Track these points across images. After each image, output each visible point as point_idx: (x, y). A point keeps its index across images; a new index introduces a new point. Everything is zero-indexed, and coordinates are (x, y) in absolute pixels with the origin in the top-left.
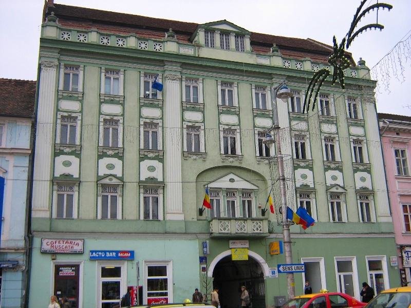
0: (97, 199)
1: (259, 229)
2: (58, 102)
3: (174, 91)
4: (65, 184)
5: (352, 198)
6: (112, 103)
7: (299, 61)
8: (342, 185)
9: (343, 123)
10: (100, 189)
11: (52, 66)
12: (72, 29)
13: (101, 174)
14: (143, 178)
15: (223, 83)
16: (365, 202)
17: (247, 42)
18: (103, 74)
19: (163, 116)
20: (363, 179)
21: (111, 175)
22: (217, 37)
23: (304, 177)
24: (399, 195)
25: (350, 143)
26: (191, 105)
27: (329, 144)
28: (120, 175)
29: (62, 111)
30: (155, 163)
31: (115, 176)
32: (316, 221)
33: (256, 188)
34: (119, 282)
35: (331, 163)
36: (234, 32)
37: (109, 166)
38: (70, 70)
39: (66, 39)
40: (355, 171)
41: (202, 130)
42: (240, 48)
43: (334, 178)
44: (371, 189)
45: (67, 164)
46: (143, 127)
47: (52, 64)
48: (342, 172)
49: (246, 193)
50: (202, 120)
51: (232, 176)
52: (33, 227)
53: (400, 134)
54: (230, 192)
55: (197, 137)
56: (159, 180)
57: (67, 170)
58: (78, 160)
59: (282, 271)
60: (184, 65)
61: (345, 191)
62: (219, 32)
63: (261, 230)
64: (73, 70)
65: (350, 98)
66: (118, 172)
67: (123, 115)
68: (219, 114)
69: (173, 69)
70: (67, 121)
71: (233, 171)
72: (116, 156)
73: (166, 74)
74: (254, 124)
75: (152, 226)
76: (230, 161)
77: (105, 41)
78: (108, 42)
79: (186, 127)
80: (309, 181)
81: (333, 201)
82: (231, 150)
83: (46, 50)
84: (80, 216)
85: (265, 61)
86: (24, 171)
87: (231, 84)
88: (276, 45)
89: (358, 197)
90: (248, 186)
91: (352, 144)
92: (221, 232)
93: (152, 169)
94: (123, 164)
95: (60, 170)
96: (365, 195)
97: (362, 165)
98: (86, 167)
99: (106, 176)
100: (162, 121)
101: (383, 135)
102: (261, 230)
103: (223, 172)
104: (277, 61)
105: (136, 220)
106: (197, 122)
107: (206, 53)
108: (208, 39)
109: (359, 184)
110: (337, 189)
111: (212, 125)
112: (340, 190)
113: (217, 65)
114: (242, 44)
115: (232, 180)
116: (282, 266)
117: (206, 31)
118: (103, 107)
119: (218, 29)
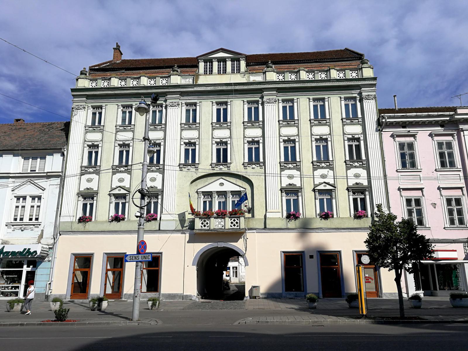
1: (207, 226)
2: (85, 134)
3: (272, 112)
4: (88, 196)
6: (95, 132)
10: (317, 193)
11: (175, 105)
12: (98, 78)
13: (317, 182)
17: (243, 63)
18: (120, 110)
19: (103, 138)
20: (290, 177)
27: (289, 146)
28: (332, 182)
30: (325, 171)
31: (328, 184)
33: (127, 192)
36: (228, 58)
38: (317, 102)
39: (135, 85)
41: (329, 141)
42: (236, 70)
44: (300, 186)
45: (89, 181)
46: (347, 141)
48: (131, 175)
50: (329, 133)
54: (221, 194)
57: (89, 185)
58: (129, 176)
59: (129, 260)
60: (88, 97)
68: (213, 129)
70: (288, 143)
71: (224, 177)
72: (158, 171)
73: (169, 101)
74: (181, 137)
75: (115, 226)
77: (123, 83)
78: (290, 76)
80: (297, 182)
82: (222, 156)
83: (126, 97)
87: (101, 107)
88: (271, 62)
91: (346, 142)
92: (232, 228)
93: (290, 177)
94: (131, 177)
95: (84, 185)
98: (308, 178)
99: (320, 184)
101: (383, 130)
102: (238, 226)
107: (203, 80)
110: (325, 186)
113: (224, 88)
115: (222, 184)
116: (129, 256)
117: (205, 62)
118: (247, 132)
119: (215, 58)
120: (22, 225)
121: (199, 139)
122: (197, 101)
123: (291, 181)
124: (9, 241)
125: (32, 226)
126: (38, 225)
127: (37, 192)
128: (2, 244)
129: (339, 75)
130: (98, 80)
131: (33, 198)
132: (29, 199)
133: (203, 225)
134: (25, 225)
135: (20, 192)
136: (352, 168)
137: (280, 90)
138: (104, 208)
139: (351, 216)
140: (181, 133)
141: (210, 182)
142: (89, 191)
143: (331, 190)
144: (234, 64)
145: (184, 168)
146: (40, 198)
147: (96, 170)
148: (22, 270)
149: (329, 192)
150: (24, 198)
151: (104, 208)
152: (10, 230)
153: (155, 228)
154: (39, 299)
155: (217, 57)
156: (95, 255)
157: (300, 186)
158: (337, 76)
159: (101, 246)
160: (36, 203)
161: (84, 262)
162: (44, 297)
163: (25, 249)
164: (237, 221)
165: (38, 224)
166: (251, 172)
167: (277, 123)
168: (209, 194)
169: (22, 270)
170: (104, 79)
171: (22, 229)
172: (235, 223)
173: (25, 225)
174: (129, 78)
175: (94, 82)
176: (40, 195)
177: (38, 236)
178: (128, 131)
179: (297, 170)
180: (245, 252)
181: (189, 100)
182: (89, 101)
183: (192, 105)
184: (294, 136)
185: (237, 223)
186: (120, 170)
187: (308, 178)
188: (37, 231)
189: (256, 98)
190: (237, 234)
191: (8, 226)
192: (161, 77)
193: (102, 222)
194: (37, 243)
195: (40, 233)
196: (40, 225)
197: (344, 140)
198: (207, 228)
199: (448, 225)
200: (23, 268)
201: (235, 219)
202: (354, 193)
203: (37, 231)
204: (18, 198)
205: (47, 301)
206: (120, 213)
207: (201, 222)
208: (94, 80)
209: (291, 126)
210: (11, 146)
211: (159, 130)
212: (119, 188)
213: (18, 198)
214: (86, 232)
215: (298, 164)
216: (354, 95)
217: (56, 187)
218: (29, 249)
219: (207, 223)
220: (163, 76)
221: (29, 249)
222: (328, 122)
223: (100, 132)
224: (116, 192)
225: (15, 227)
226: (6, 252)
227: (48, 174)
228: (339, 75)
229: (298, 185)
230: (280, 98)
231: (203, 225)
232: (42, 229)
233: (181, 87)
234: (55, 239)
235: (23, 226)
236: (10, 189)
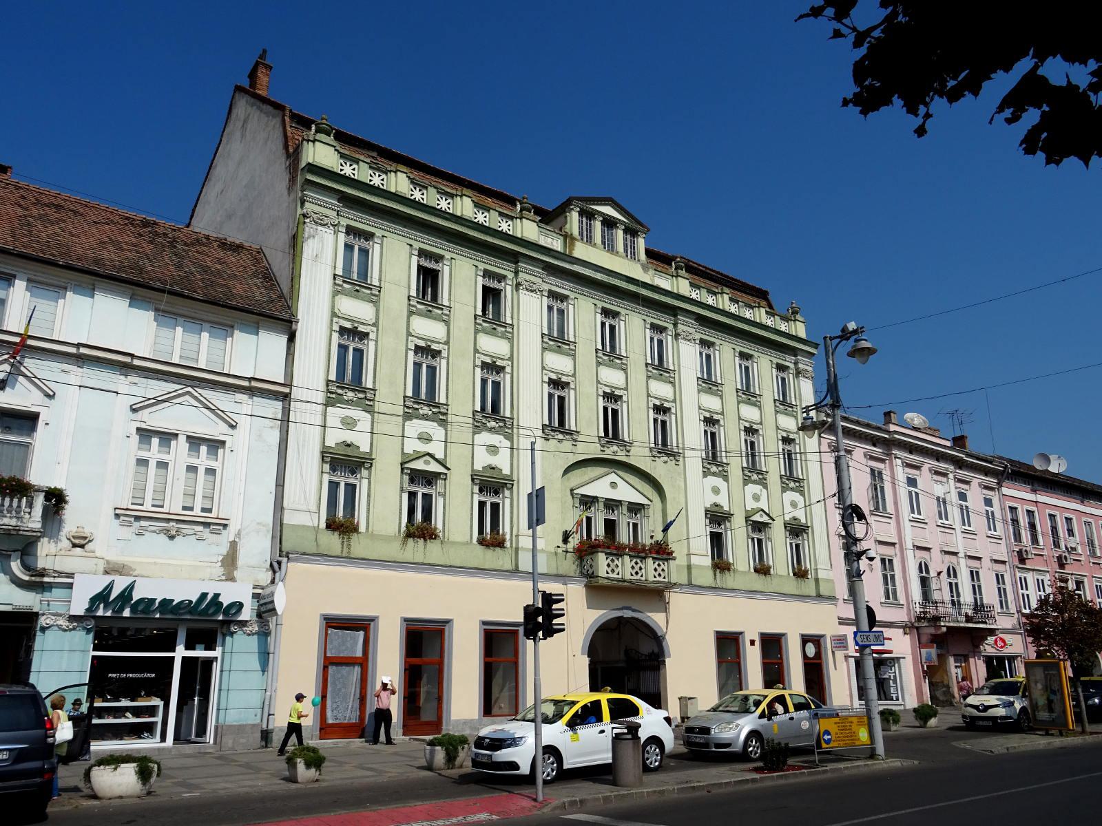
0: (401, 497)
4: (345, 463)
5: (778, 534)
6: (357, 298)
7: (378, 169)
8: (440, 456)
9: (768, 406)
13: (409, 449)
14: (478, 467)
15: (350, 230)
16: (490, 500)
20: (493, 450)
21: (428, 454)
22: (598, 225)
23: (794, 505)
24: (138, 429)
25: (407, 353)
26: (557, 340)
29: (339, 317)
30: (497, 439)
32: (362, 528)
34: (183, 658)
35: (425, 400)
36: (623, 223)
37: (423, 438)
40: (746, 482)
42: (631, 253)
43: (756, 498)
44: (509, 473)
47: (691, 337)
49: (635, 508)
51: (613, 477)
52: (554, 572)
53: (877, 445)
54: (611, 505)
55: (358, 354)
56: (504, 472)
60: (346, 200)
61: (445, 471)
62: (623, 227)
63: (618, 574)
64: (493, 281)
65: (606, 312)
66: (437, 449)
67: (375, 324)
69: (687, 326)
71: (620, 473)
75: (416, 550)
76: (612, 452)
79: (547, 380)
80: (502, 462)
81: (414, 489)
84: (370, 529)
85: (664, 283)
86: (272, 427)
89: (476, 489)
90: (638, 499)
91: (335, 336)
92: (655, 579)
93: (493, 450)
96: (796, 530)
97: (495, 420)
100: (510, 363)
102: (618, 574)
103: (599, 470)
104: (683, 286)
105: (466, 544)
106: (364, 324)
108: (587, 231)
109: (482, 460)
110: (761, 516)
111: (589, 383)
112: (434, 467)
113: (623, 284)
114: (589, 231)
119: (600, 213)
120: (169, 520)
121: (675, 403)
122: (572, 295)
123: (349, 436)
124: (133, 567)
125: (200, 528)
126: (221, 528)
127: (210, 427)
128: (106, 572)
129: (342, 168)
130: (361, 163)
131: (195, 442)
132: (181, 444)
133: (610, 568)
134: (178, 521)
135: (157, 419)
136: (417, 418)
137: (703, 321)
138: (382, 503)
139: (400, 531)
140: (542, 355)
141: (636, 486)
142: (349, 451)
143: (437, 475)
144: (582, 221)
145: (659, 457)
146: (216, 445)
147: (366, 398)
148: (173, 657)
149: (429, 478)
150: (167, 437)
151: (382, 503)
152: (127, 533)
153: (502, 566)
154: (243, 741)
155: (603, 213)
156: (456, 626)
157: (509, 473)
158: (338, 167)
159: (391, 598)
160: (203, 459)
161: (424, 641)
162: (259, 735)
163: (204, 595)
164: (640, 564)
165: (220, 525)
166: (660, 469)
167: (331, 281)
168: (588, 502)
169: (173, 657)
170: (710, 292)
171: (173, 533)
172: (637, 568)
173: (178, 521)
174: (435, 188)
175: (348, 164)
176: (222, 438)
177: (221, 558)
178: (435, 319)
179: (440, 425)
180: (665, 630)
181: (556, 286)
182: (346, 211)
183: (360, 236)
184: (439, 343)
185: (641, 569)
186: (421, 412)
187: (390, 438)
188: (217, 546)
189: (664, 321)
190: (656, 595)
191: (122, 518)
192: (501, 214)
193: (386, 539)
194: (224, 578)
195: (224, 550)
196: (225, 526)
197: (407, 349)
198: (617, 576)
199: (883, 600)
200: (174, 651)
201: (661, 563)
202: (333, 469)
203: (217, 546)
204: (145, 434)
205: (266, 747)
206: (340, 513)
207: (606, 563)
208: (350, 160)
209: (712, 393)
210: (80, 259)
211: (500, 335)
212: (427, 458)
213: (145, 434)
214: (430, 565)
215: (369, 396)
216: (787, 364)
217: (271, 424)
218: (217, 596)
219: (641, 569)
220: (505, 212)
221: (217, 596)
222: (509, 333)
223: (372, 302)
224: (419, 465)
225: (143, 523)
226: (141, 601)
227: (254, 384)
228: (342, 168)
229: (365, 448)
230: (344, 222)
231: (610, 568)
232: (231, 539)
233: (552, 253)
234: (274, 572)
235: (171, 524)
236: (124, 402)
